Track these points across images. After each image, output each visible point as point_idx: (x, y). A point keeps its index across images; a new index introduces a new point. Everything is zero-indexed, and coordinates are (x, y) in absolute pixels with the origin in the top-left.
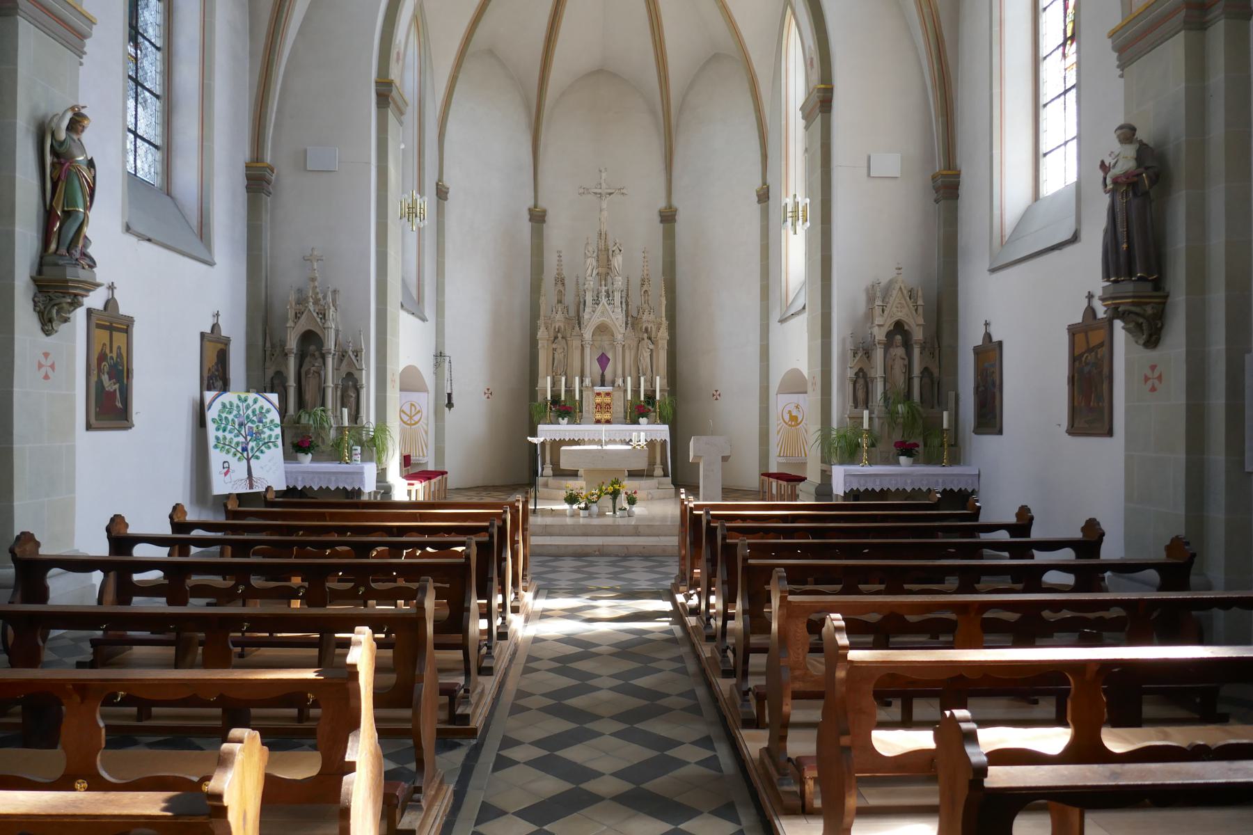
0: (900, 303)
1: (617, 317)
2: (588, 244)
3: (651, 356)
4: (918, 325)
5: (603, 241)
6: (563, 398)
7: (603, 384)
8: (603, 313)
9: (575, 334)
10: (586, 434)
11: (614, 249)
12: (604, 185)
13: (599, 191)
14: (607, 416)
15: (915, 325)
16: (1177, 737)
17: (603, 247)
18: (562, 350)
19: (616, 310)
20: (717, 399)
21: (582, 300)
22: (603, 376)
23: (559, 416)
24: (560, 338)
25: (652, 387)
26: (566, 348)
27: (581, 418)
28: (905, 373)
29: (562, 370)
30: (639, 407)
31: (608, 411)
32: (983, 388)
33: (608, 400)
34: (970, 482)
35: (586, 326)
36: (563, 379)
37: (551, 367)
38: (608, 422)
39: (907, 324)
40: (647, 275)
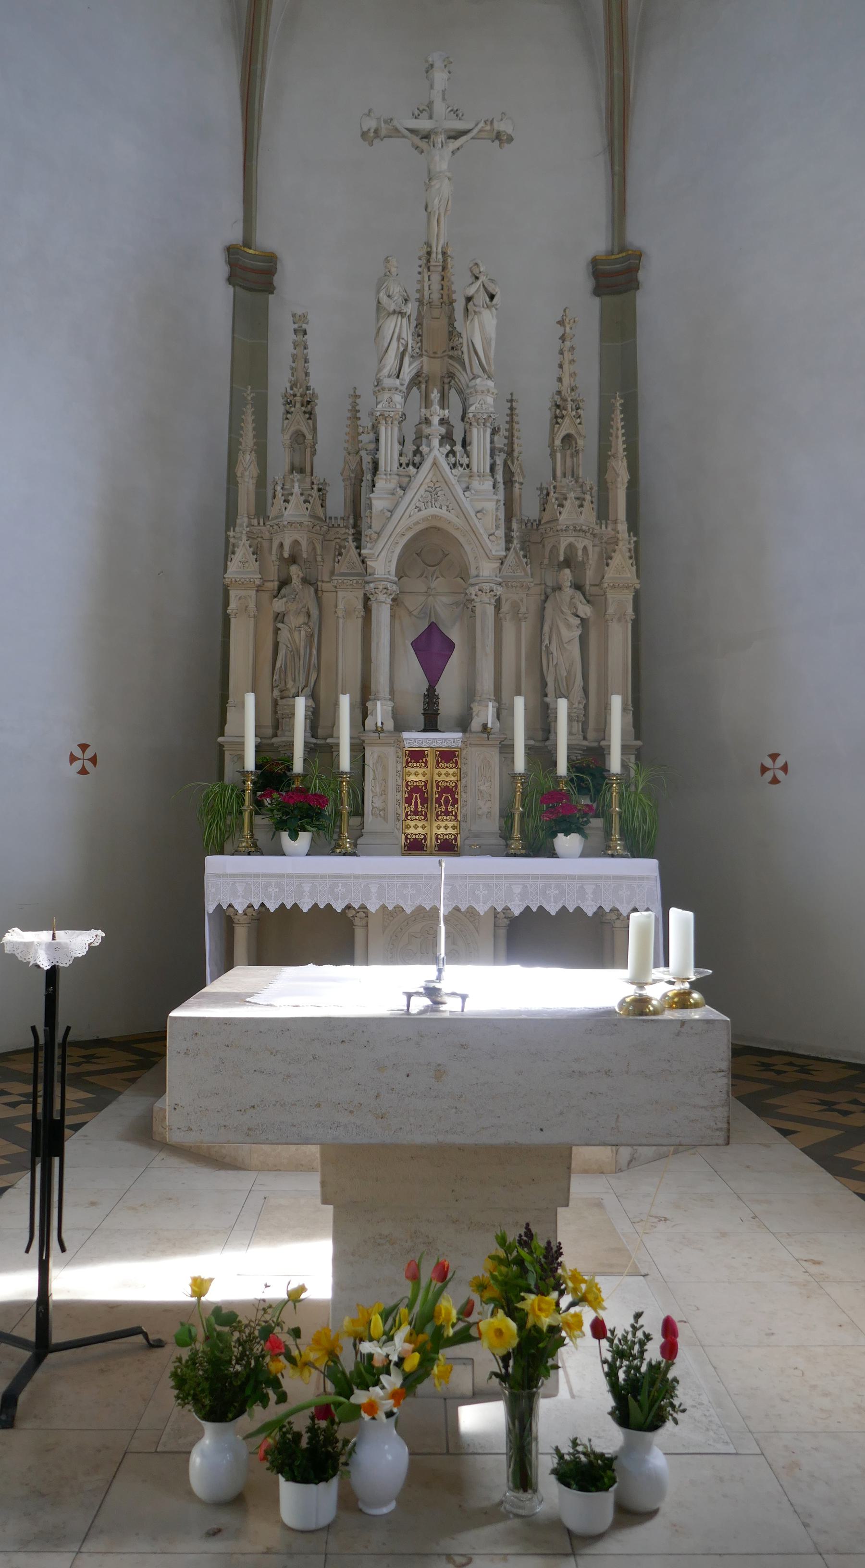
1: (479, 506)
2: (387, 274)
3: (583, 641)
5: (436, 278)
6: (298, 766)
7: (431, 723)
8: (433, 493)
9: (344, 570)
10: (374, 889)
11: (471, 291)
12: (440, 108)
13: (424, 124)
14: (444, 828)
17: (436, 296)
18: (302, 619)
19: (475, 484)
20: (775, 781)
21: (367, 459)
22: (431, 699)
23: (281, 825)
24: (296, 581)
25: (585, 738)
26: (315, 612)
27: (358, 833)
29: (302, 679)
30: (553, 797)
31: (447, 813)
33: (446, 775)
35: (379, 534)
36: (301, 704)
37: (267, 669)
38: (447, 847)
40: (572, 390)
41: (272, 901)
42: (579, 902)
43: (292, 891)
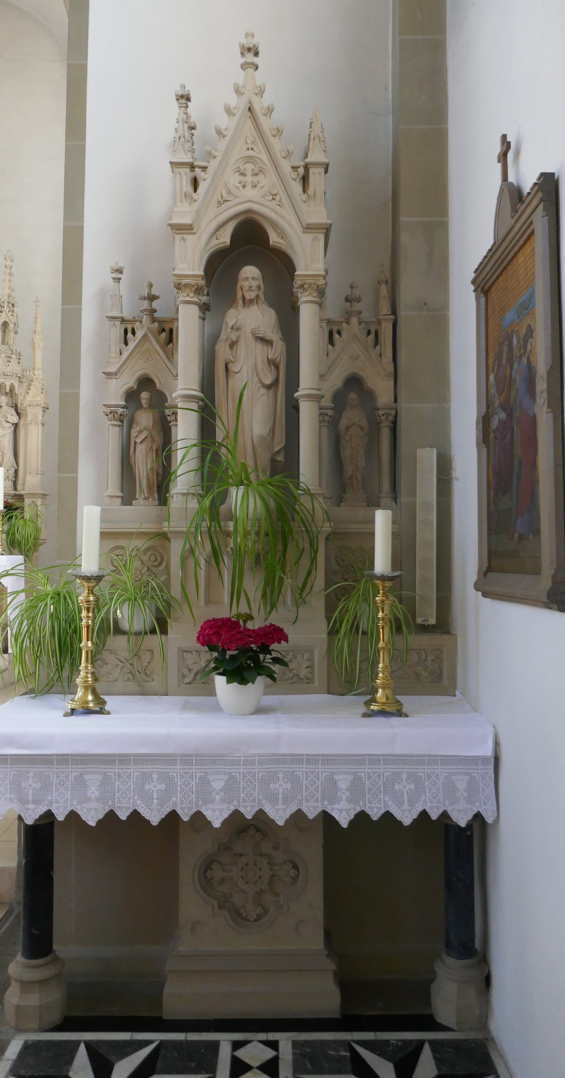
0: (250, 160)
4: (309, 228)
15: (299, 229)
28: (273, 386)
32: (503, 415)
34: (461, 784)
39: (275, 225)
41: (280, 806)
42: (326, 803)
43: (317, 789)
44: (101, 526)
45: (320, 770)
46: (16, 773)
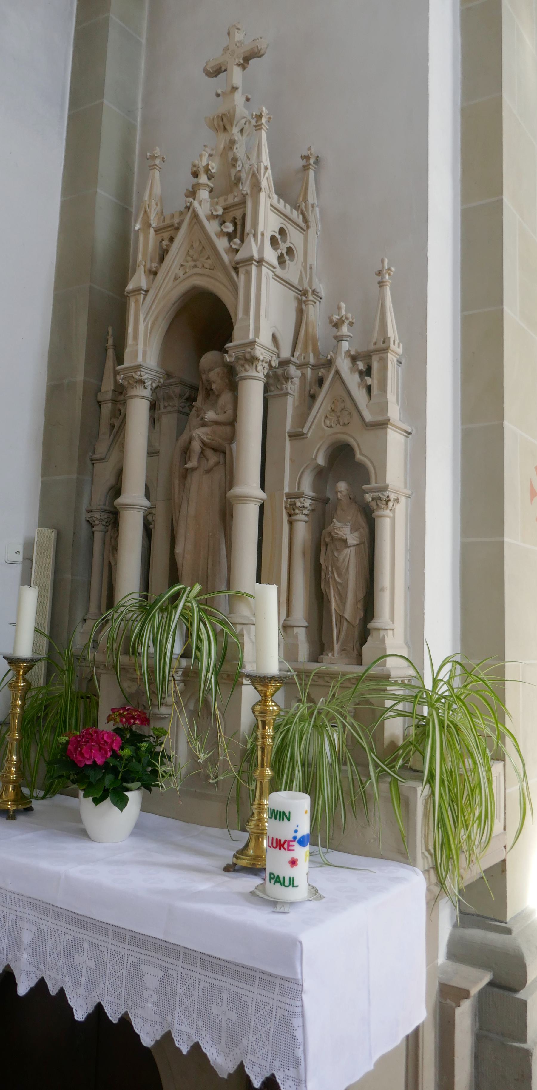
16: (34, 914)
44: (148, 450)
45: (127, 952)
46: (207, 985)
